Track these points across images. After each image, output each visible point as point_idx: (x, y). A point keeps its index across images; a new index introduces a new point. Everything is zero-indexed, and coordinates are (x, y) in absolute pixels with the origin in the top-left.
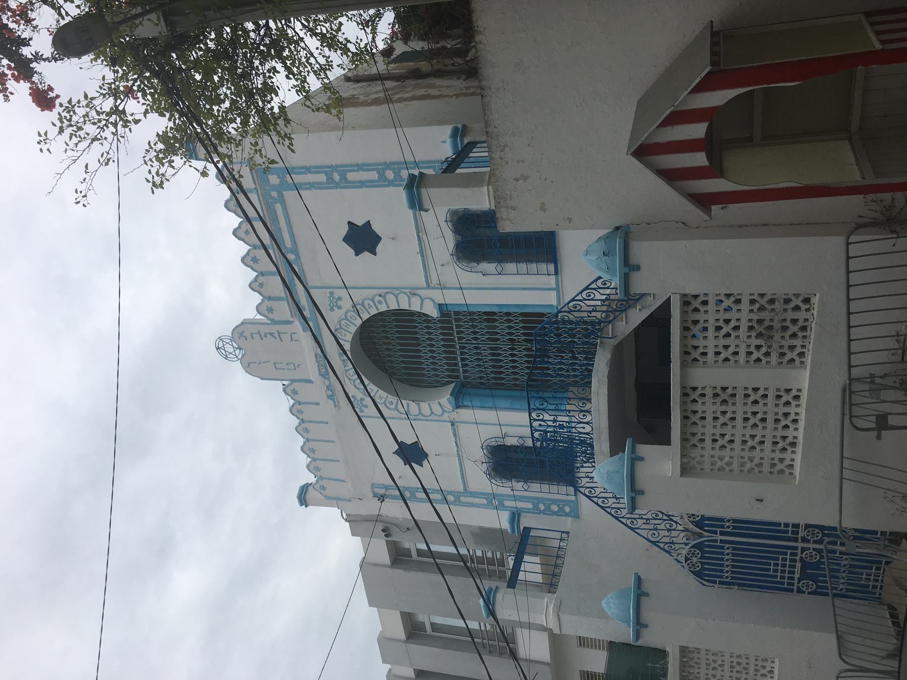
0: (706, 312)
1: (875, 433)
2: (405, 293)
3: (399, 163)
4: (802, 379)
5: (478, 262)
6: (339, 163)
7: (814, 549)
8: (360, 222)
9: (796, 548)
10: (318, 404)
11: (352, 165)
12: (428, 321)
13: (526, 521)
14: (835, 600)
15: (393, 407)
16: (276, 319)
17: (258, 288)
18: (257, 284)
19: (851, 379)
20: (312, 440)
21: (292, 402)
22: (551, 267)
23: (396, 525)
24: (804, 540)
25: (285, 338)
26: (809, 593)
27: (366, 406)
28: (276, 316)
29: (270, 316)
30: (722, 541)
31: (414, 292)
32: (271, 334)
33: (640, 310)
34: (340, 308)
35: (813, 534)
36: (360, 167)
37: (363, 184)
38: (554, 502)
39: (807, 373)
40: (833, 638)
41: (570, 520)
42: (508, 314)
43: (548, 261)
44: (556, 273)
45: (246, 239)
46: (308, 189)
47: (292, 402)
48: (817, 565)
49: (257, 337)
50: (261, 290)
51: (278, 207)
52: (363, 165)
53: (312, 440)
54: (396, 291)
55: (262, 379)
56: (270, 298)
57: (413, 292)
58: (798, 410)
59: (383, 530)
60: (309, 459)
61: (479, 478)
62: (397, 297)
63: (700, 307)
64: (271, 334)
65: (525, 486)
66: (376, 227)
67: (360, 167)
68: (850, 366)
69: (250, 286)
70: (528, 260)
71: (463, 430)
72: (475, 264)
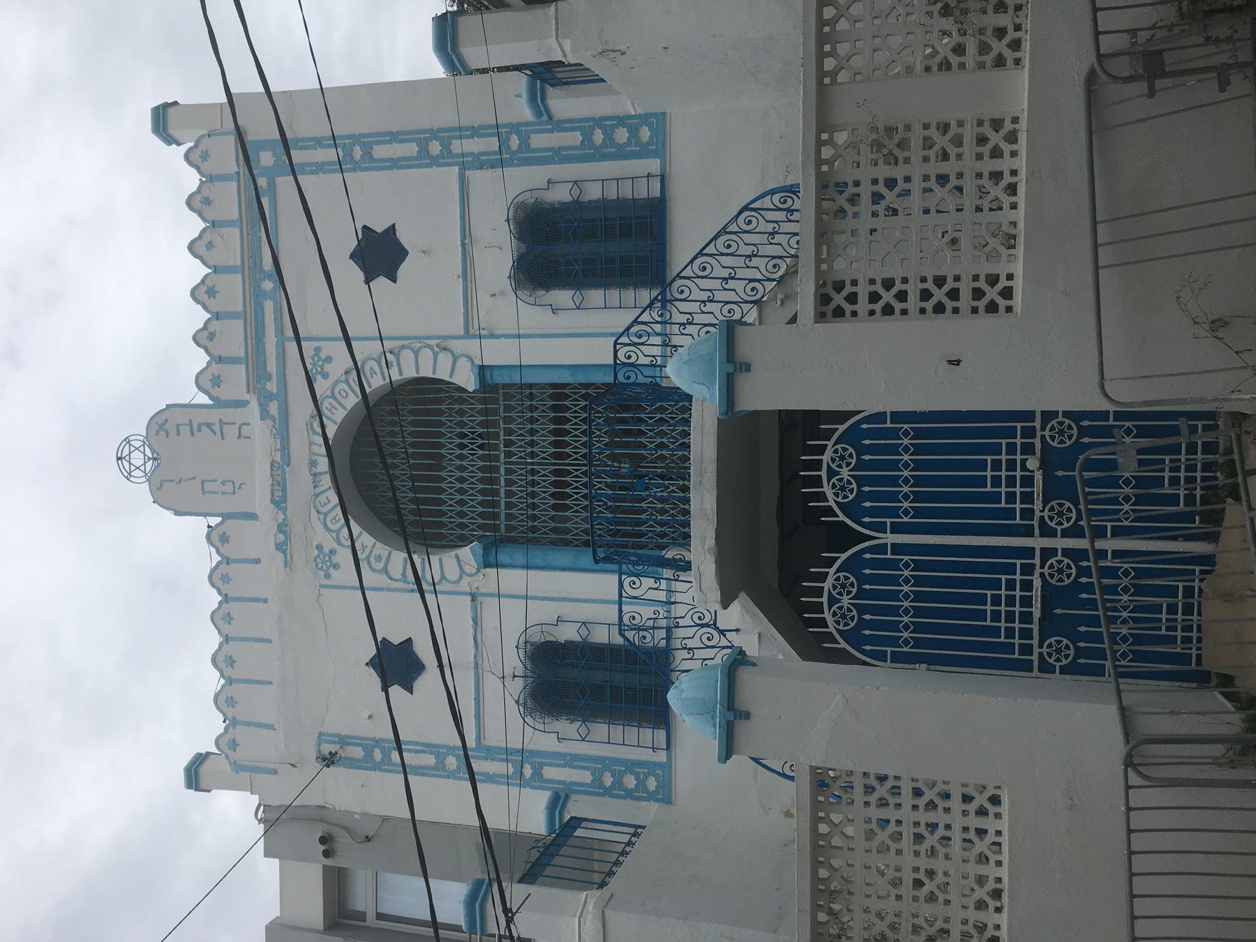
0: (947, 810)
1: (1142, 87)
2: (431, 347)
3: (450, 130)
4: (1016, 92)
5: (547, 287)
6: (367, 130)
7: (1066, 552)
8: (379, 228)
9: (1029, 552)
10: (257, 561)
11: (384, 134)
12: (462, 401)
13: (577, 807)
14: (1120, 680)
15: (380, 566)
16: (223, 398)
17: (205, 342)
18: (206, 333)
19: (1100, 57)
20: (234, 639)
22: (662, 734)
24: (1047, 532)
25: (231, 432)
26: (1064, 671)
27: (336, 566)
28: (224, 393)
29: (216, 392)
30: (897, 548)
31: (443, 345)
32: (209, 425)
33: (782, 302)
34: (332, 552)
36: (395, 137)
37: (395, 163)
38: (631, 766)
39: (1025, 74)
40: (1112, 710)
41: (654, 807)
43: (650, 285)
44: (668, 747)
46: (312, 172)
47: (201, 225)
49: (185, 430)
50: (210, 345)
52: (399, 133)
53: (234, 639)
54: (417, 342)
55: (177, 513)
57: (442, 344)
59: (323, 840)
60: (222, 681)
61: (503, 717)
62: (416, 353)
63: (938, 801)
64: (209, 425)
66: (403, 236)
67: (395, 137)
68: (1097, 34)
69: (195, 339)
70: (621, 203)
71: (489, 609)
72: (543, 292)
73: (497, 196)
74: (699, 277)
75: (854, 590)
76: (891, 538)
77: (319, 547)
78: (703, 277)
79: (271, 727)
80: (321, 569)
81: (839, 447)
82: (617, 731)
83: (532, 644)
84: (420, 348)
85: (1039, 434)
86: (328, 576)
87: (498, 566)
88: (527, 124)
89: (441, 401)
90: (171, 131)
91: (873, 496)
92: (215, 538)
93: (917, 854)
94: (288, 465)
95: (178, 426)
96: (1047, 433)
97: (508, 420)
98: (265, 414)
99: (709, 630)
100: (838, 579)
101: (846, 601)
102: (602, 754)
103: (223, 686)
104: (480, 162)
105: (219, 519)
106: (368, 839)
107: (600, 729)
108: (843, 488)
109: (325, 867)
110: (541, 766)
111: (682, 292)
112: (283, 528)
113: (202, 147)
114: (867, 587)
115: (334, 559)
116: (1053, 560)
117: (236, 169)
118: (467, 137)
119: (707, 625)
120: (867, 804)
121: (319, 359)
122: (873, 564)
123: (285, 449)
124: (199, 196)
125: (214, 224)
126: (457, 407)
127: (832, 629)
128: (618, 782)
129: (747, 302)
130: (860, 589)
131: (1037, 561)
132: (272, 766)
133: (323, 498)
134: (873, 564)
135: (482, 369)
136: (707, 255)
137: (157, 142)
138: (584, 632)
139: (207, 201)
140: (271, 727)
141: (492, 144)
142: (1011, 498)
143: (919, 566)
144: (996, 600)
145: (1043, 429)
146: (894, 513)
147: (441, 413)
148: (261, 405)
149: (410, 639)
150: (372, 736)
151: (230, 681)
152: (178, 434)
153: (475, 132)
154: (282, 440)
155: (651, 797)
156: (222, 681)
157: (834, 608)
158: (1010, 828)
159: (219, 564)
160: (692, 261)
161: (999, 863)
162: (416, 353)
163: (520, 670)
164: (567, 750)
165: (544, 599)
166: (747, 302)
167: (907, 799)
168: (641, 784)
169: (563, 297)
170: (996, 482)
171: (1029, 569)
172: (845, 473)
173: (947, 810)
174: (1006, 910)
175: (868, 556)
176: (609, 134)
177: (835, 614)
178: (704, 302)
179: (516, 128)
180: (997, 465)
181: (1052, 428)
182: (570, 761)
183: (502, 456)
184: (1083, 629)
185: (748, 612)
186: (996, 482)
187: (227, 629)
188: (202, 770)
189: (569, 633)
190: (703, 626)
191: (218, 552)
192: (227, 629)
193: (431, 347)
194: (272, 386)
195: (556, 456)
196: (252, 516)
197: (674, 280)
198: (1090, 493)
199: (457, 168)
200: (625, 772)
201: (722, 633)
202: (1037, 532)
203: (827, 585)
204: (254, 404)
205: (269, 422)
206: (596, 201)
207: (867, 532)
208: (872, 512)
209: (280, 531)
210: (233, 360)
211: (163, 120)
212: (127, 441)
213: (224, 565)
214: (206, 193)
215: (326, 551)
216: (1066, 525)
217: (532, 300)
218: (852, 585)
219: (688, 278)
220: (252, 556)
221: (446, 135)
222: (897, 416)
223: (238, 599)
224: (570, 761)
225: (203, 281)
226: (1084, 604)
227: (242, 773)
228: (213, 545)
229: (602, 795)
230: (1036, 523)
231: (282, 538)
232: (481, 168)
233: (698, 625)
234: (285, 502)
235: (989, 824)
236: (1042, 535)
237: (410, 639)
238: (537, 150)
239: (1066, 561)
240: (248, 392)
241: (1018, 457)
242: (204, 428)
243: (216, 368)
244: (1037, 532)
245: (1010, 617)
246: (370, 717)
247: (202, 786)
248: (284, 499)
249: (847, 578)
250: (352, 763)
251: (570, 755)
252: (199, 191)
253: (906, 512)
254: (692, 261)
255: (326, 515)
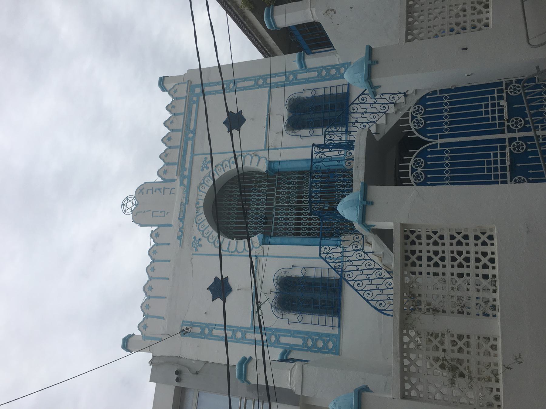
2: (250, 155)
7: (520, 139)
9: (504, 140)
10: (169, 244)
20: (154, 278)
21: (153, 243)
22: (336, 320)
23: (189, 368)
24: (510, 131)
25: (167, 191)
27: (200, 246)
28: (167, 177)
30: (442, 145)
31: (255, 154)
34: (200, 240)
35: (517, 123)
36: (245, 79)
38: (321, 336)
44: (339, 326)
46: (214, 94)
47: (153, 243)
48: (524, 157)
49: (150, 192)
51: (195, 106)
53: (154, 278)
55: (141, 225)
57: (255, 153)
58: (487, 15)
59: (177, 373)
64: (159, 189)
65: (311, 132)
66: (244, 114)
70: (331, 95)
73: (281, 98)
74: (361, 103)
75: (423, 165)
76: (439, 141)
77: (195, 238)
79: (163, 318)
80: (194, 247)
82: (316, 318)
85: (505, 91)
86: (196, 250)
89: (251, 182)
90: (165, 85)
92: (154, 235)
93: (453, 266)
94: (188, 204)
96: (508, 91)
98: (182, 184)
100: (416, 161)
101: (419, 170)
102: (308, 330)
103: (146, 300)
104: (277, 85)
106: (197, 373)
107: (308, 318)
108: (418, 123)
109: (176, 387)
111: (354, 109)
112: (181, 230)
113: (175, 88)
114: (429, 163)
115: (200, 243)
116: (515, 143)
119: (359, 250)
120: (428, 244)
122: (432, 153)
123: (187, 197)
125: (174, 115)
128: (315, 345)
129: (381, 113)
130: (425, 164)
131: (507, 144)
133: (199, 217)
134: (432, 153)
135: (270, 163)
137: (158, 89)
139: (173, 107)
140: (163, 318)
141: (283, 79)
142: (494, 119)
143: (452, 151)
145: (507, 89)
146: (441, 130)
147: (251, 187)
148: (180, 180)
151: (149, 297)
153: (276, 75)
155: (330, 352)
156: (146, 298)
157: (414, 173)
158: (498, 242)
159: (153, 246)
160: (358, 97)
161: (494, 268)
163: (274, 289)
164: (291, 329)
165: (287, 257)
166: (381, 113)
167: (447, 240)
169: (305, 132)
170: (487, 113)
171: (503, 148)
172: (419, 117)
173: (467, 244)
174: (498, 291)
175: (429, 150)
176: (328, 72)
177: (414, 176)
178: (363, 113)
179: (292, 72)
180: (487, 106)
181: (511, 88)
182: (293, 333)
183: (275, 203)
184: (530, 171)
186: (487, 113)
187: (149, 293)
188: (130, 340)
189: (297, 273)
190: (357, 250)
191: (154, 241)
192: (149, 293)
193: (250, 155)
194: (186, 173)
196: (170, 225)
197: (351, 105)
198: (528, 93)
200: (318, 339)
201: (366, 253)
202: (506, 131)
203: (411, 164)
207: (429, 140)
208: (431, 131)
209: (180, 230)
210: (173, 164)
211: (162, 82)
212: (127, 198)
213: (166, 166)
214: (173, 104)
216: (520, 127)
217: (293, 134)
218: (422, 163)
219: (357, 104)
221: (264, 78)
222: (441, 91)
223: (159, 261)
224: (293, 333)
225: (167, 135)
226: (530, 160)
227: (146, 340)
228: (152, 238)
229: (307, 351)
230: (506, 128)
231: (180, 233)
232: (278, 87)
234: (184, 219)
235: (488, 249)
236: (508, 133)
238: (299, 80)
239: (521, 142)
241: (496, 102)
242: (157, 190)
244: (506, 131)
245: (496, 169)
246: (206, 313)
249: (419, 160)
250: (195, 336)
254: (358, 97)
255: (199, 224)
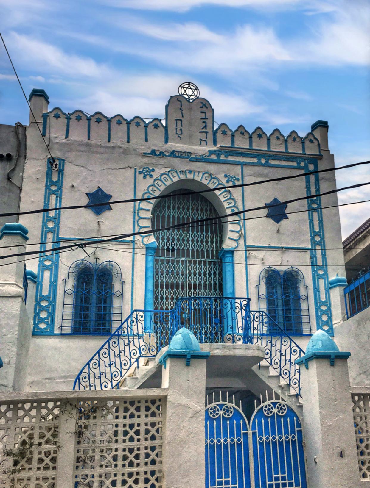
2: (241, 230)
18: (244, 131)
20: (109, 125)
21: (147, 122)
22: (68, 331)
28: (219, 135)
29: (220, 132)
30: (246, 435)
34: (151, 176)
38: (52, 315)
42: (156, 298)
44: (62, 335)
45: (273, 136)
47: (147, 122)
49: (203, 116)
50: (239, 132)
51: (295, 164)
53: (109, 125)
56: (233, 136)
62: (141, 218)
64: (205, 127)
76: (250, 432)
77: (153, 170)
78: (291, 351)
80: (143, 170)
81: (233, 410)
83: (112, 269)
84: (240, 225)
86: (140, 173)
87: (147, 255)
88: (328, 278)
89: (212, 233)
90: (319, 129)
91: (266, 423)
92: (157, 122)
93: (124, 450)
94: (190, 160)
95: (205, 113)
97: (205, 262)
98: (211, 152)
99: (138, 354)
102: (57, 301)
105: (164, 125)
106: (9, 179)
108: (269, 409)
110: (51, 270)
113: (315, 141)
114: (228, 422)
117: (307, 153)
118: (322, 252)
119: (140, 352)
121: (235, 180)
123: (196, 160)
124: (244, 131)
126: (209, 240)
127: (262, 405)
128: (42, 309)
129: (281, 370)
130: (227, 419)
132: (47, 135)
133: (175, 174)
136: (300, 353)
137: (314, 121)
138: (118, 294)
139: (294, 140)
144: (283, 478)
146: (261, 433)
148: (215, 151)
149: (112, 209)
150: (63, 186)
152: (202, 112)
154: (200, 159)
159: (145, 122)
162: (141, 218)
166: (281, 370)
168: (42, 320)
172: (275, 410)
175: (242, 422)
177: (215, 407)
179: (326, 273)
182: (54, 285)
183: (189, 259)
185: (147, 372)
188: (43, 99)
190: (140, 350)
191: (150, 123)
193: (241, 230)
194: (222, 158)
195: (190, 285)
197: (290, 338)
199: (310, 247)
200: (48, 313)
201: (137, 360)
203: (227, 403)
204: (215, 148)
205: (207, 154)
206: (300, 306)
207: (251, 421)
208: (260, 423)
209: (161, 153)
215: (152, 173)
218: (282, 413)
220: (148, 138)
224: (54, 285)
225: (264, 133)
227: (42, 118)
228: (153, 121)
229: (36, 301)
231: (158, 153)
233: (140, 348)
237: (112, 209)
240: (220, 146)
242: (204, 125)
243: (229, 133)
246: (73, 186)
247: (34, 98)
248: (175, 157)
249: (231, 412)
251: (57, 284)
252: (299, 137)
253: (261, 439)
254: (297, 346)
255: (168, 175)
